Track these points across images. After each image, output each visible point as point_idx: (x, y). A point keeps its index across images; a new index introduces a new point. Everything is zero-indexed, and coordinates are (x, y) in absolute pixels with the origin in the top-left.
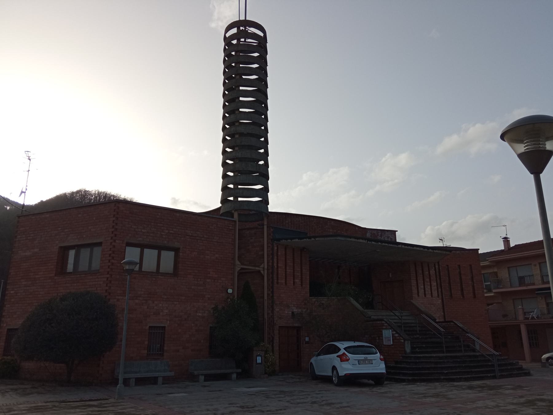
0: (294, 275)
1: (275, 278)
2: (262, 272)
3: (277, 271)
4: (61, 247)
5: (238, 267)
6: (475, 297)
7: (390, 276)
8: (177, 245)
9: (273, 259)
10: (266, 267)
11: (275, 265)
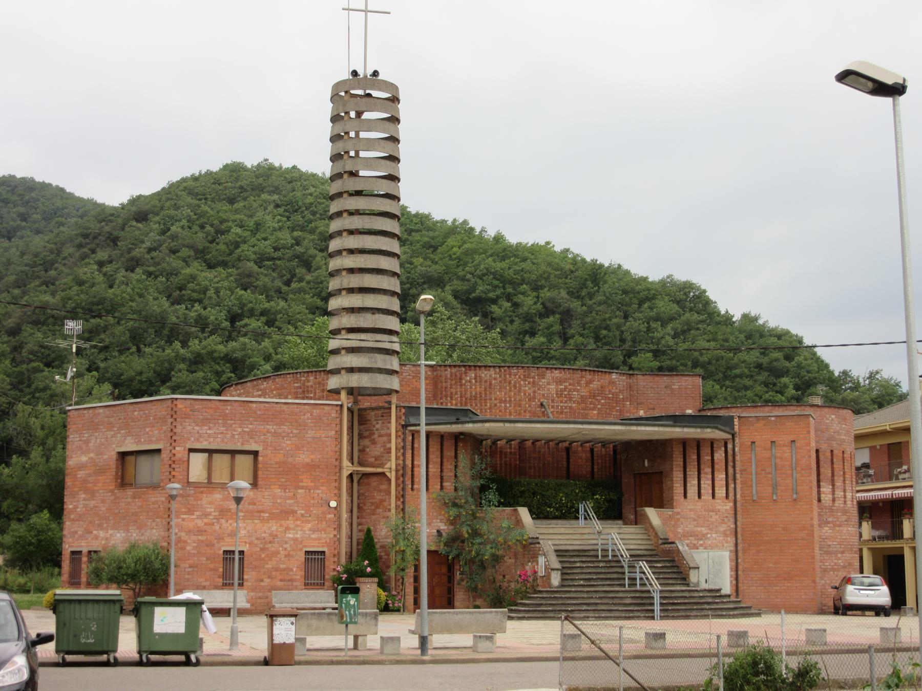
0: (442, 478)
1: (409, 483)
2: (388, 474)
3: (412, 471)
4: (119, 453)
5: (348, 468)
6: (713, 497)
7: (646, 464)
8: (253, 447)
9: (404, 454)
10: (394, 467)
11: (409, 462)
